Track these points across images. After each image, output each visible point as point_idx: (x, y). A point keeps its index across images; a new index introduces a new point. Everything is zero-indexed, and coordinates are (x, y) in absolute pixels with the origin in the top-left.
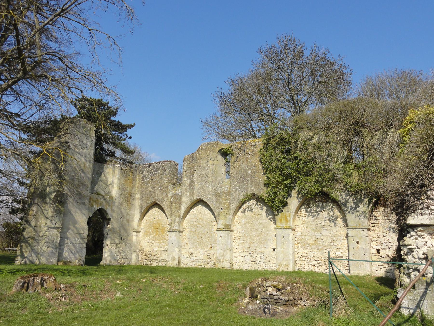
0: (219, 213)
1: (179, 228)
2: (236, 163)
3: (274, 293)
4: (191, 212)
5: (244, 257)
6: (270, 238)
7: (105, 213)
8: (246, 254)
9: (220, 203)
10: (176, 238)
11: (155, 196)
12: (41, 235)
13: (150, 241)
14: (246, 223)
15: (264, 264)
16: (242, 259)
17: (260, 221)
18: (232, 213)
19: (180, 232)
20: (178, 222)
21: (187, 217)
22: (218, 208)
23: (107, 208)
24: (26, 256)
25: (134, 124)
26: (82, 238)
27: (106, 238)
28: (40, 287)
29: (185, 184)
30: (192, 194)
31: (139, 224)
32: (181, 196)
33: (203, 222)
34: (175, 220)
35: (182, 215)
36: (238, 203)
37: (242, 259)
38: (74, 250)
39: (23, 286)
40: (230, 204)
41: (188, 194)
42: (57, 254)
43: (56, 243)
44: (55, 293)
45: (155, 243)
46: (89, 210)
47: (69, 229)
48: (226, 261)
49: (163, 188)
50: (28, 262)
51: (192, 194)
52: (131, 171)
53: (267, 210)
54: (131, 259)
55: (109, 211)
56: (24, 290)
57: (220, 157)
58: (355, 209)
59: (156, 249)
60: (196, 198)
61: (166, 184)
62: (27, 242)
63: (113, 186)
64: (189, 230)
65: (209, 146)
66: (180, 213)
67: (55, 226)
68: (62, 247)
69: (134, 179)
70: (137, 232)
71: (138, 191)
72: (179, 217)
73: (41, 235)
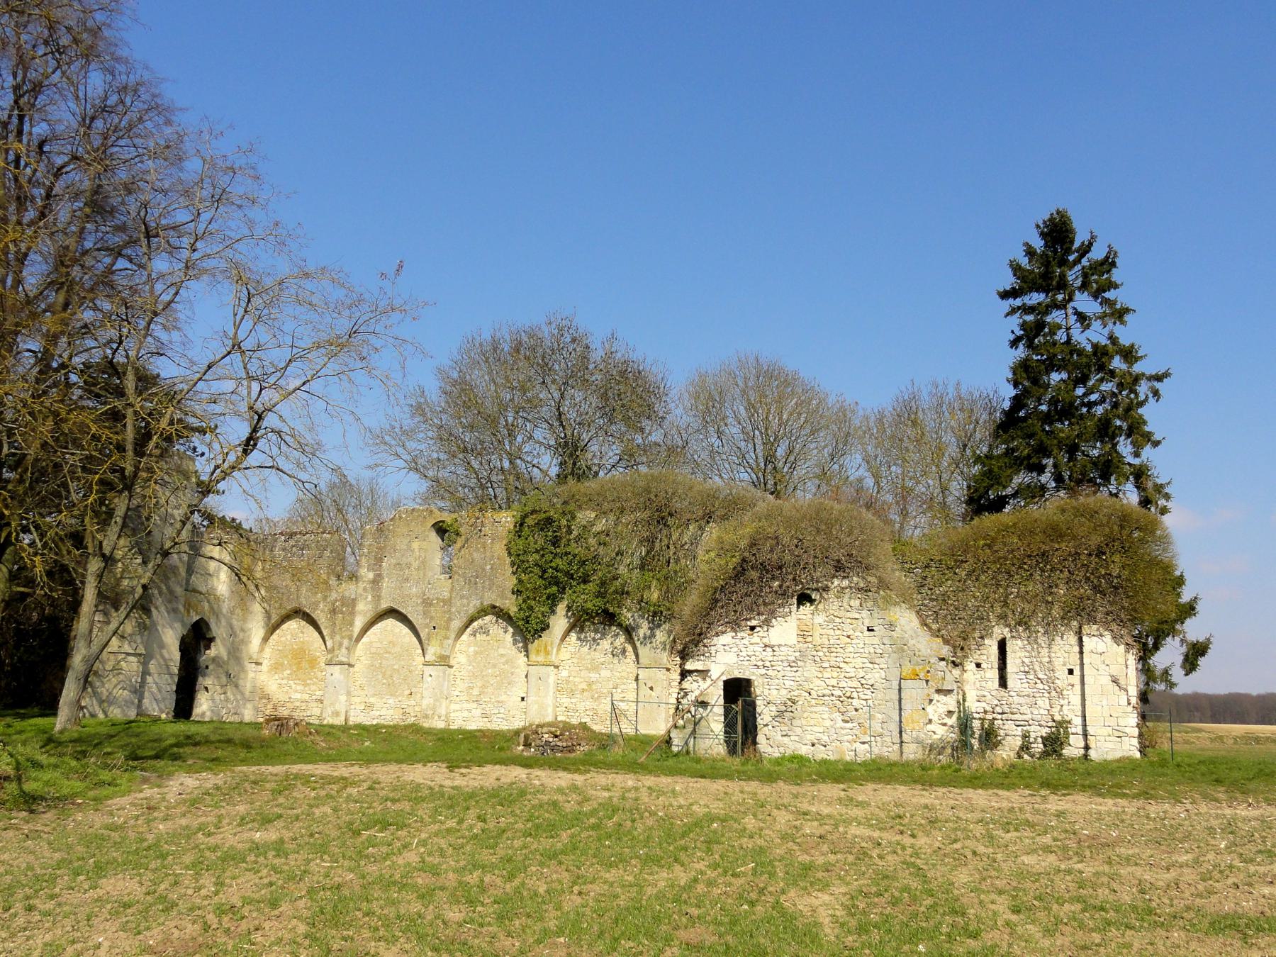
0: (429, 634)
5: (470, 711)
6: (517, 680)
7: (205, 630)
8: (475, 705)
9: (432, 618)
13: (285, 682)
14: (476, 653)
15: (505, 723)
16: (466, 714)
17: (502, 651)
21: (365, 640)
22: (427, 625)
26: (171, 675)
27: (204, 675)
30: (377, 598)
31: (261, 650)
33: (397, 649)
34: (341, 645)
35: (355, 635)
37: (466, 714)
38: (159, 697)
40: (450, 620)
41: (370, 598)
45: (294, 686)
48: (439, 717)
51: (377, 598)
53: (514, 634)
55: (213, 626)
57: (434, 536)
60: (385, 605)
65: (414, 513)
67: (138, 651)
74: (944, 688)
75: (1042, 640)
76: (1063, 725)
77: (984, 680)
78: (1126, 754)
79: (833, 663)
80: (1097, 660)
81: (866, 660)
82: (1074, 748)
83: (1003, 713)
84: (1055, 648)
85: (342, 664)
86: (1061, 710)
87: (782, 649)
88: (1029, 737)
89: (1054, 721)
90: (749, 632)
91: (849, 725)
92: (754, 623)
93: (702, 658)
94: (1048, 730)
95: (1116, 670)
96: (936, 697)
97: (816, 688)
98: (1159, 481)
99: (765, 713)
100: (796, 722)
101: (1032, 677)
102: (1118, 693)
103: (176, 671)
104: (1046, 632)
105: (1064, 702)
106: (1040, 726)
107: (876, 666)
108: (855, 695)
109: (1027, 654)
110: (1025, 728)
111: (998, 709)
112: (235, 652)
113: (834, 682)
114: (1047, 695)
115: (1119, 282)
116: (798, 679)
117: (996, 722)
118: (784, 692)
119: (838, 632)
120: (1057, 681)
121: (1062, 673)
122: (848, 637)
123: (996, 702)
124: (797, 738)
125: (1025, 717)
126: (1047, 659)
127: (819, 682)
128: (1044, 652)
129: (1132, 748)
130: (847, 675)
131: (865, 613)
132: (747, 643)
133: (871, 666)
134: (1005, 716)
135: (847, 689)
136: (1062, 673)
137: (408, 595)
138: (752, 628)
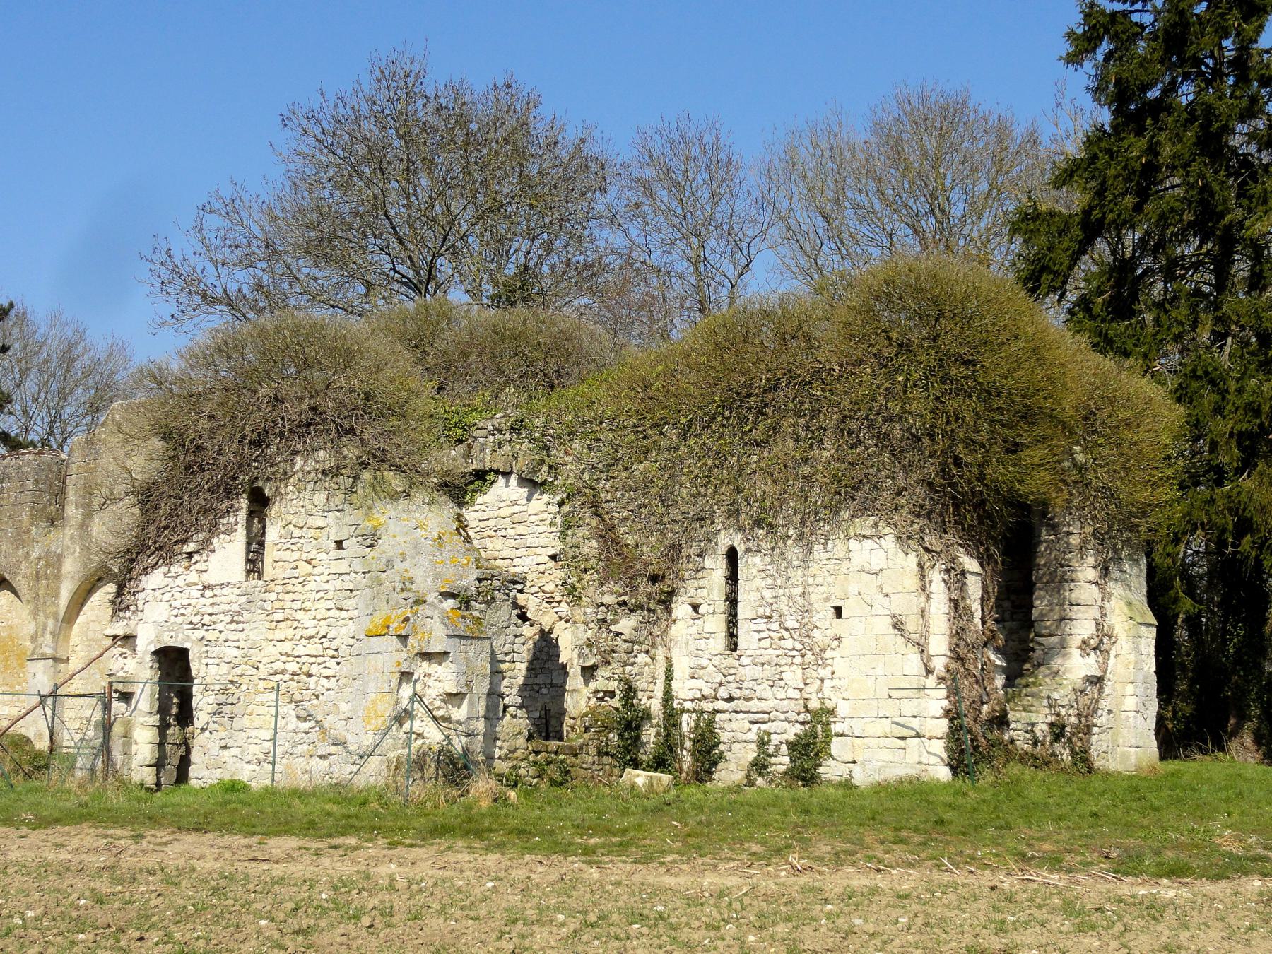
1: (55, 649)
4: (89, 603)
20: (53, 634)
29: (73, 522)
34: (45, 629)
35: (62, 611)
49: (19, 534)
58: (933, 567)
61: (26, 521)
64: (82, 654)
66: (58, 606)
72: (56, 619)
75: (793, 551)
76: (823, 716)
77: (703, 636)
79: (289, 613)
81: (330, 604)
83: (730, 699)
84: (814, 568)
85: (44, 658)
86: (820, 690)
87: (225, 591)
88: (768, 743)
89: (808, 711)
90: (185, 562)
91: (306, 726)
93: (128, 614)
94: (799, 729)
96: (425, 667)
97: (265, 660)
99: (202, 704)
100: (238, 723)
101: (775, 626)
104: (800, 536)
107: (344, 614)
108: (314, 669)
109: (769, 582)
110: (764, 727)
111: (723, 693)
113: (287, 647)
114: (798, 660)
116: (242, 644)
117: (718, 717)
119: (296, 555)
120: (816, 633)
121: (824, 616)
123: (719, 678)
125: (763, 706)
127: (270, 649)
129: (933, 760)
132: (182, 584)
136: (824, 616)
138: (190, 555)
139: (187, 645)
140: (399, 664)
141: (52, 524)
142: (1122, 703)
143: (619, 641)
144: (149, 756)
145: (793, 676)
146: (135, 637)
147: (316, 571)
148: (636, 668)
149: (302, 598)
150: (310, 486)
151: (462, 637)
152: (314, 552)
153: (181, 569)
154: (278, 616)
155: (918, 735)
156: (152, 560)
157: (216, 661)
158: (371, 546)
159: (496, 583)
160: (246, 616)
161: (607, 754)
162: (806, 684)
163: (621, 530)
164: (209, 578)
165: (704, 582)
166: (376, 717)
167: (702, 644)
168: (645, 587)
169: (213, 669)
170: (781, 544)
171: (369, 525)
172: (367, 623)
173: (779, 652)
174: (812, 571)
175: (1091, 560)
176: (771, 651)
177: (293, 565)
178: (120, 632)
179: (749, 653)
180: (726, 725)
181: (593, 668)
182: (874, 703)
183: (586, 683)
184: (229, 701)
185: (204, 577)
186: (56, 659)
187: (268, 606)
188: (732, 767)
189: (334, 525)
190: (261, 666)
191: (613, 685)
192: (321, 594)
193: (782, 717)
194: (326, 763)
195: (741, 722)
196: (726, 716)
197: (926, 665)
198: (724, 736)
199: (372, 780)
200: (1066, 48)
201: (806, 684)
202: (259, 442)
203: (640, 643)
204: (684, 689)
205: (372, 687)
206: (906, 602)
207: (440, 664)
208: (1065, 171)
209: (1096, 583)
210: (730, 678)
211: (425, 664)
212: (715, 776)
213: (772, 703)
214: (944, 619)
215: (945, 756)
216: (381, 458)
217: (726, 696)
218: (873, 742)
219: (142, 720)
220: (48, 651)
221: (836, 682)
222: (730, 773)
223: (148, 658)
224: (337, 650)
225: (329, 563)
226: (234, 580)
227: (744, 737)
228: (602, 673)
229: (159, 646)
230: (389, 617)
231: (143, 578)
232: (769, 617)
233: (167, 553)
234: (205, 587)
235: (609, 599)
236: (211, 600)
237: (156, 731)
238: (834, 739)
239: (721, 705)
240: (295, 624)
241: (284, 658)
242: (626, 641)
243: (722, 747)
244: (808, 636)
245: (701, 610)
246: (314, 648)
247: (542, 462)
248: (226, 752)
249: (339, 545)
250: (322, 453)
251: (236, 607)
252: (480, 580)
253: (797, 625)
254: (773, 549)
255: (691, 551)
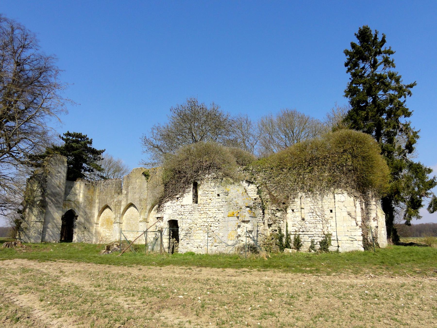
2: (151, 181)
3: (116, 247)
9: (142, 206)
10: (117, 227)
11: (107, 201)
12: (31, 226)
13: (104, 230)
18: (148, 212)
19: (120, 223)
20: (119, 218)
21: (125, 214)
23: (75, 209)
24: (22, 238)
25: (105, 150)
26: (58, 228)
28: (14, 246)
30: (127, 200)
32: (121, 201)
33: (134, 217)
34: (117, 216)
35: (121, 213)
36: (151, 206)
39: (6, 246)
40: (147, 206)
42: (41, 237)
43: (41, 231)
44: (20, 248)
46: (63, 211)
47: (49, 223)
50: (23, 242)
51: (127, 200)
52: (92, 185)
54: (92, 241)
56: (7, 247)
57: (144, 177)
59: (107, 234)
60: (129, 202)
61: (113, 194)
62: (22, 230)
63: (79, 196)
65: (138, 170)
66: (120, 212)
68: (44, 233)
69: (95, 190)
70: (97, 224)
71: (97, 198)
73: (31, 226)
74: (245, 220)
75: (319, 197)
76: (328, 236)
77: (295, 217)
78: (357, 249)
79: (205, 211)
80: (341, 205)
81: (216, 209)
82: (332, 248)
83: (303, 232)
84: (324, 201)
85: (117, 223)
86: (327, 229)
87: (187, 206)
88: (314, 242)
89: (324, 234)
90: (176, 200)
92: (178, 196)
93: (161, 212)
94: (322, 239)
95: (351, 209)
96: (243, 224)
97: (198, 223)
98: (414, 131)
99: (181, 234)
100: (191, 238)
101: (314, 214)
102: (351, 220)
103: (61, 227)
104: (320, 194)
105: (329, 225)
106: (319, 237)
107: (220, 212)
108: (212, 225)
109: (312, 204)
110: (312, 238)
111: (301, 230)
112: (88, 220)
113: (205, 220)
114: (321, 222)
115: (394, 51)
116: (192, 219)
117: (300, 236)
118: (187, 225)
119: (207, 198)
120: (325, 216)
121: (327, 212)
122: (210, 199)
124: (191, 245)
125: (312, 233)
126: (321, 206)
127: (199, 220)
128: (320, 203)
129: (360, 246)
130: (210, 216)
131: (216, 189)
132: (176, 205)
133: (218, 211)
134: (304, 233)
135: (210, 222)
136: (327, 212)
137: (135, 198)
138: (178, 198)
139: (177, 219)
140: (237, 223)
141: (119, 194)
142: (381, 232)
143: (277, 218)
144: (167, 246)
145: (320, 226)
146: (163, 217)
147: (212, 201)
148: (281, 224)
149: (209, 208)
150: (210, 181)
151: (252, 217)
152: (211, 197)
153: (175, 201)
154: (202, 212)
155: (356, 240)
156: (167, 199)
157: (185, 223)
158: (227, 195)
159: (257, 204)
160: (193, 212)
161: (277, 245)
162: (323, 228)
163: (273, 193)
164: (182, 203)
165: (294, 204)
166: (231, 236)
167: (295, 219)
168: (282, 205)
169: (184, 225)
170: (315, 195)
171: (227, 190)
172: (227, 214)
173: (316, 220)
174: (323, 202)
175: (374, 200)
176: (313, 220)
177: (206, 200)
178: (159, 216)
179: (308, 221)
180: (303, 238)
181: (271, 224)
182: (344, 232)
183: (269, 228)
184: (189, 232)
185: (181, 203)
186: (120, 223)
187: (199, 210)
188: (305, 248)
189: (217, 191)
190: (197, 224)
191: (277, 228)
192: (214, 207)
193: (317, 236)
194: (216, 248)
195: (306, 237)
196: (302, 235)
197: (356, 223)
198: (302, 240)
199: (231, 252)
200: (344, 94)
201: (323, 228)
202: (197, 172)
203: (282, 219)
204: (290, 229)
205: (230, 229)
206: (351, 209)
207: (247, 223)
208: (345, 119)
209: (375, 205)
210: (303, 227)
211: (243, 223)
212: (300, 249)
213: (314, 232)
214: (360, 212)
215: (362, 245)
216: (227, 175)
217: (302, 231)
218: (344, 242)
219: (165, 237)
220: (118, 221)
221: (332, 228)
222: (304, 249)
223: (167, 222)
224: (219, 220)
225: (216, 200)
226: (190, 204)
227: (307, 240)
228: (273, 226)
229: (170, 220)
230: (233, 212)
231: (165, 203)
232: (313, 212)
233: (171, 198)
234: (182, 206)
235: (274, 208)
236: (184, 209)
237: (168, 240)
238: (332, 241)
239: (301, 233)
240: (207, 214)
241: (204, 222)
242: (279, 218)
243: (301, 243)
244: (324, 217)
245: (294, 211)
246: (212, 220)
247: (252, 177)
248: (188, 245)
249: (218, 195)
250: (213, 174)
251: (190, 210)
252: (254, 203)
253: (320, 214)
254: (313, 196)
255: (291, 197)
